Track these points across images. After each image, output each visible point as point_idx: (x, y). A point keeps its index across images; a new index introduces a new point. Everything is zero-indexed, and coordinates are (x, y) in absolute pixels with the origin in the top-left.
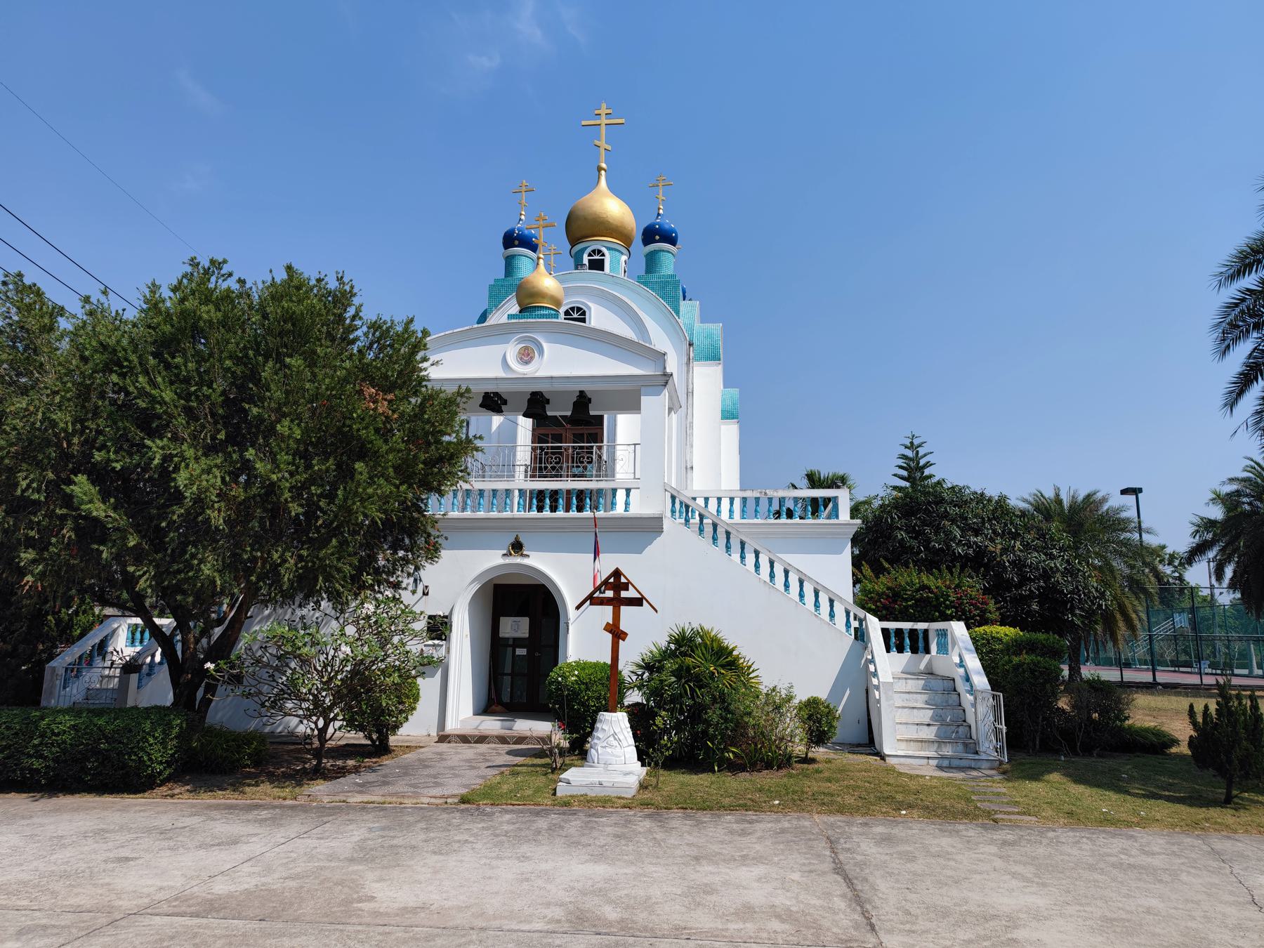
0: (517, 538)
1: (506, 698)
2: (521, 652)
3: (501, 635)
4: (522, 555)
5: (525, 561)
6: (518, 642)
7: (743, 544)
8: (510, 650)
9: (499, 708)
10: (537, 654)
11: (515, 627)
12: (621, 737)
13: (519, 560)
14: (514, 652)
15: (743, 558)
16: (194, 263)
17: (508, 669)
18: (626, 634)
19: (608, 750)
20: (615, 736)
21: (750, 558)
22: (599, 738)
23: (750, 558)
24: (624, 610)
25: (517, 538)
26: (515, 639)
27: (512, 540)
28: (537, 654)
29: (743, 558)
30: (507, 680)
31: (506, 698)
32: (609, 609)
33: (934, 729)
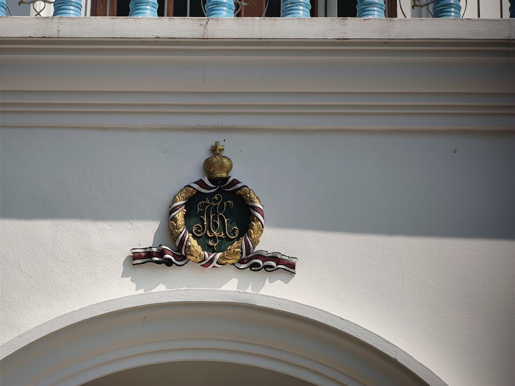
5: (272, 292)
13: (229, 285)
27: (188, 172)
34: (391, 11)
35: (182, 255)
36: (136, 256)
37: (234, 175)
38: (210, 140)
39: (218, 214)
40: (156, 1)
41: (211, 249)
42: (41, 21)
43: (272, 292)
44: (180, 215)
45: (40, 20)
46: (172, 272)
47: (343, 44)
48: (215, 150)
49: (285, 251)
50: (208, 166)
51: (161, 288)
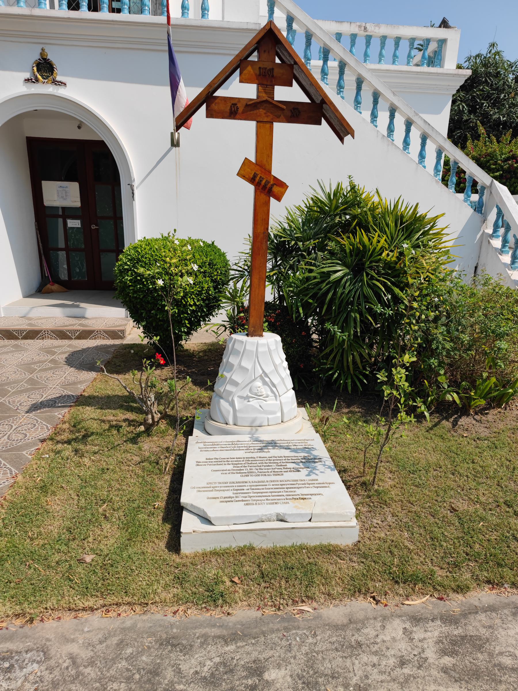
0: (43, 50)
1: (64, 276)
2: (74, 223)
3: (46, 203)
4: (55, 82)
5: (61, 91)
6: (67, 213)
7: (376, 96)
8: (60, 220)
9: (56, 287)
10: (94, 227)
11: (61, 194)
12: (276, 380)
13: (50, 89)
14: (65, 224)
15: (374, 116)
16: (145, 238)
17: (62, 244)
18: (283, 186)
19: (254, 403)
20: (260, 363)
21: (383, 117)
22: (235, 384)
23: (383, 117)
24: (282, 130)
25: (43, 53)
26: (64, 209)
27: (37, 57)
28: (94, 227)
29: (374, 116)
30: (62, 255)
31: (64, 276)
32: (246, 130)
33: (467, 281)
34: (52, 6)
35: (37, 80)
36: (26, 80)
37: (48, 57)
38: (41, 46)
39: (45, 68)
40: (138, 1)
41: (44, 79)
42: (208, 641)
43: (61, 91)
44: (35, 68)
45: (45, 10)
46: (35, 85)
47: (69, 19)
48: (43, 50)
49: (63, 81)
50: (41, 54)
51: (33, 89)
